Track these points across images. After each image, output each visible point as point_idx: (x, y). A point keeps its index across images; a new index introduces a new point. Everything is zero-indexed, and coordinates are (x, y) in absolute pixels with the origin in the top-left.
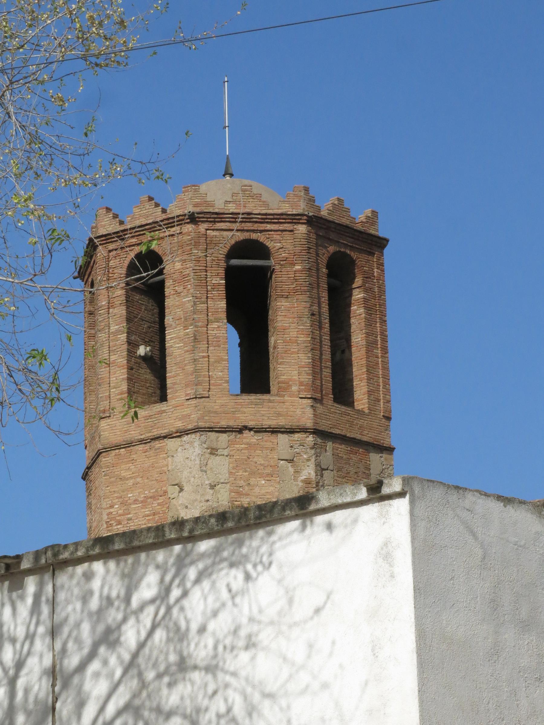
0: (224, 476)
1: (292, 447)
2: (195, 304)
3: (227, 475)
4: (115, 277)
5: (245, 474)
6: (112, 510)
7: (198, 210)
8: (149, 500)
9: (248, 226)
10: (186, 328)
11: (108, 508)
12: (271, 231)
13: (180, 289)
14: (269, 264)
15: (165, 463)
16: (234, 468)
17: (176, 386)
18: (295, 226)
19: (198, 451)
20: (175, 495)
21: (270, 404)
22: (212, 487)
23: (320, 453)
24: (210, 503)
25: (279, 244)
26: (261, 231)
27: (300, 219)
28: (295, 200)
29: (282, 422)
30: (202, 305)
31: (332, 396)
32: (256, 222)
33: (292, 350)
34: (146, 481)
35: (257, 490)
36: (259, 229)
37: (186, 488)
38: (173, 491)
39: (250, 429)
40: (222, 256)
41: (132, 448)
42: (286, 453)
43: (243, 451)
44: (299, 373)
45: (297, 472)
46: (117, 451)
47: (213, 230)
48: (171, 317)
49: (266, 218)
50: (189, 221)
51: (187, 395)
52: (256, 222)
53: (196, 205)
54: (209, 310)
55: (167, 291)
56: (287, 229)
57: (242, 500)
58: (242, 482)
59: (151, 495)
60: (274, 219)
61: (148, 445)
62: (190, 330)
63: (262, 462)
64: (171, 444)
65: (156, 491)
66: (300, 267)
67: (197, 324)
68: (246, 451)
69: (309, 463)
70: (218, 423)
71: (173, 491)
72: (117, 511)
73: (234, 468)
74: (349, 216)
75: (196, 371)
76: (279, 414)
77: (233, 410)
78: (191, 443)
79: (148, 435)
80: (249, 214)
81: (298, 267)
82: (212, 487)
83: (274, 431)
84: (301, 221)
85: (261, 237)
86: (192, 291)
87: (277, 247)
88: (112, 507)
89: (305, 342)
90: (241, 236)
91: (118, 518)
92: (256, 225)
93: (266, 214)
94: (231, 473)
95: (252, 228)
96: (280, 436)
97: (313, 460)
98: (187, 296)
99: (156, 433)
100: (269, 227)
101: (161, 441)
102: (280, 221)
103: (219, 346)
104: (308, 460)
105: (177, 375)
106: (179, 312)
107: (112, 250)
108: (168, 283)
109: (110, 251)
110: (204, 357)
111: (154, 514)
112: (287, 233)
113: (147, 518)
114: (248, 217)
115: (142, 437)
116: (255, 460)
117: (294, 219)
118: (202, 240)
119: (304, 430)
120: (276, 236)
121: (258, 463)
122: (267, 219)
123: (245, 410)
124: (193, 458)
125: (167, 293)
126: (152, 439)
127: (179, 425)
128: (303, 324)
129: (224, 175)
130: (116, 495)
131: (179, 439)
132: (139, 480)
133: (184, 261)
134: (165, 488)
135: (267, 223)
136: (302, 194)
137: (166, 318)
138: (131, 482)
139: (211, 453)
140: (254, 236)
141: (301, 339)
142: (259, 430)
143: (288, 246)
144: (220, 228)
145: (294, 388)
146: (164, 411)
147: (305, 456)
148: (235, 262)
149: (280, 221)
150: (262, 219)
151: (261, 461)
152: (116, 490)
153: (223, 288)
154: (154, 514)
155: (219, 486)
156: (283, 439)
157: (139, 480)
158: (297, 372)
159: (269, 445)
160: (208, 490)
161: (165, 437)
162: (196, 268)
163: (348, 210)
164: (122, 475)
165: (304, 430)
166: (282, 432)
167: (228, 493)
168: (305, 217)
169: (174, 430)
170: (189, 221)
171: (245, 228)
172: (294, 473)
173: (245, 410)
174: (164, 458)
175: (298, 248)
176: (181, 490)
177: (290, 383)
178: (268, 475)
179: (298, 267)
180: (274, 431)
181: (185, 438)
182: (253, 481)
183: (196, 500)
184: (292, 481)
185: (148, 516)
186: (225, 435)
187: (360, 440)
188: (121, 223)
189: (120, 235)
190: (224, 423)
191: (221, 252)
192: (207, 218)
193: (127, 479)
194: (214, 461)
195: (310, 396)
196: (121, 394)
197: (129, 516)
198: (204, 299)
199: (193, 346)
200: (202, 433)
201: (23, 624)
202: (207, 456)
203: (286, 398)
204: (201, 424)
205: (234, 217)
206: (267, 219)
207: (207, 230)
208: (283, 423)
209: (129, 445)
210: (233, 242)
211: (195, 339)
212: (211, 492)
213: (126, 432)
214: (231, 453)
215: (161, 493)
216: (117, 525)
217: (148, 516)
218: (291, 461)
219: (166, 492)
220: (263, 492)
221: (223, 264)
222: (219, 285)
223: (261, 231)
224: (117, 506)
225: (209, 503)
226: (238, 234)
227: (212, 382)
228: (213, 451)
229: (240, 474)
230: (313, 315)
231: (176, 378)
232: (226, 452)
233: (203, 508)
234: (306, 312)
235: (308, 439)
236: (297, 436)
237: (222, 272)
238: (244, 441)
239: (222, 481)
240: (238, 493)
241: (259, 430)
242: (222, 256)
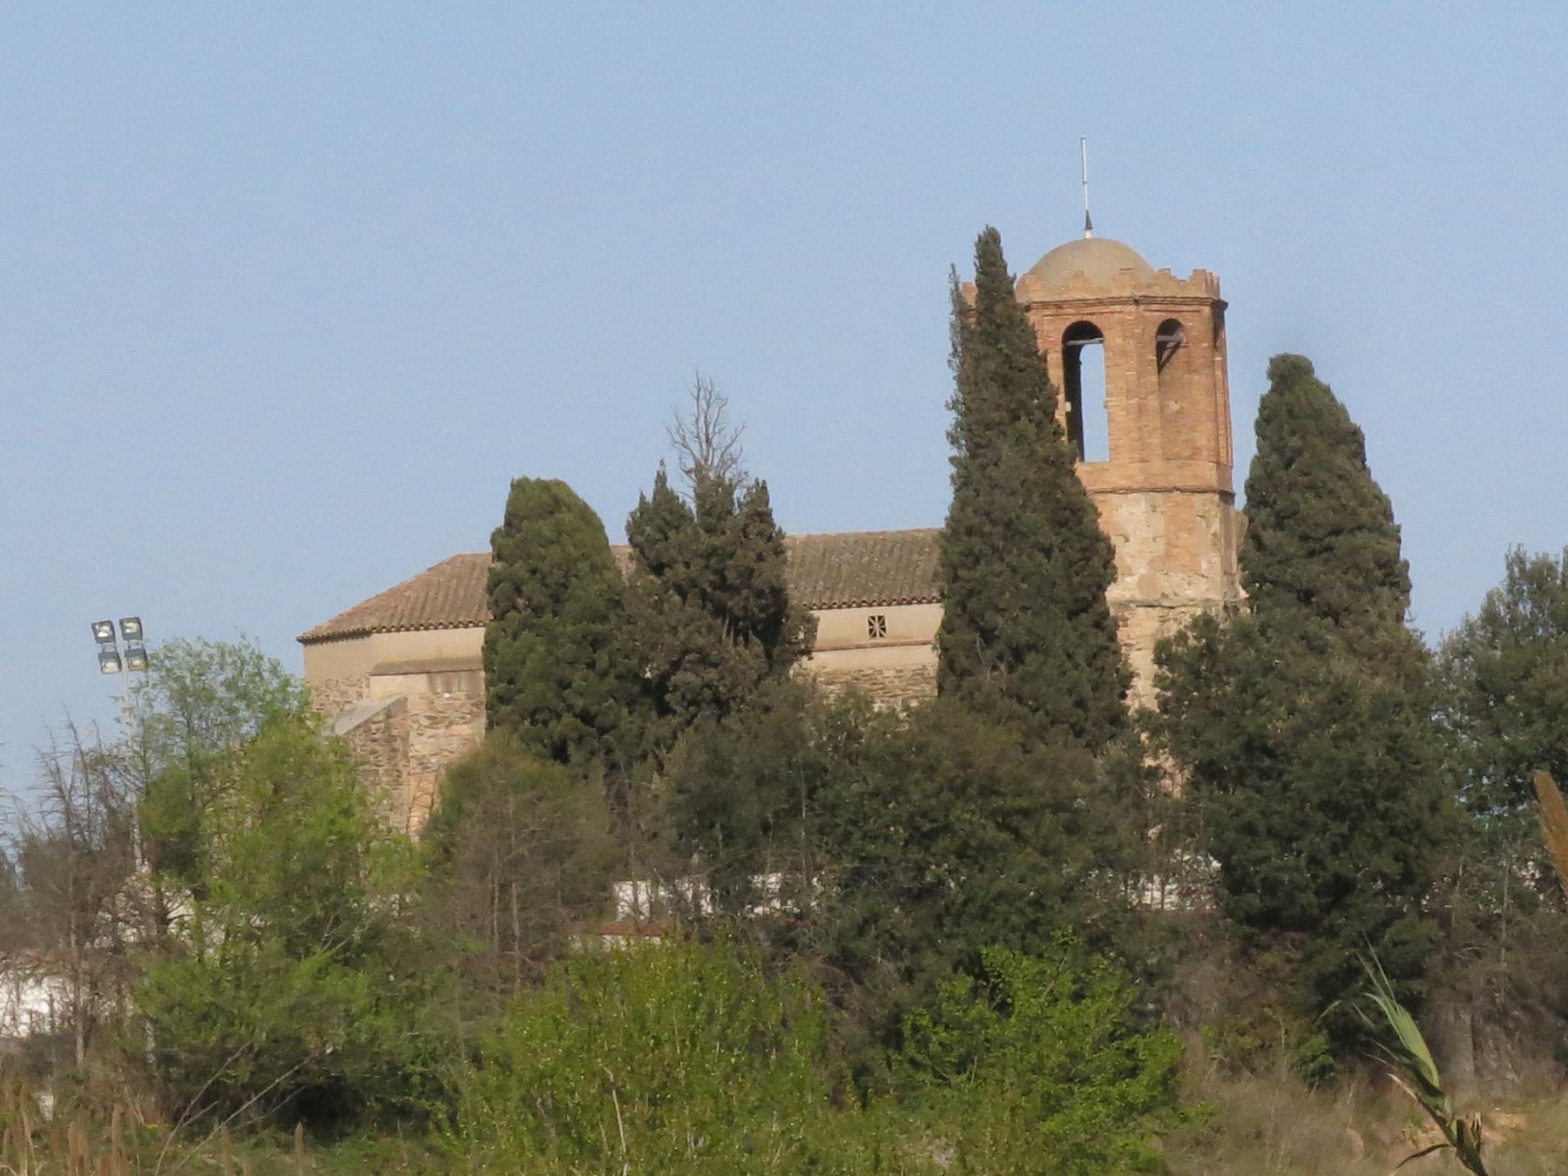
9: (1172, 308)
37: (1131, 539)
39: (1178, 490)
49: (1185, 301)
78: (1137, 501)
85: (1094, 320)
90: (1075, 319)
100: (1186, 308)
120: (1189, 315)
140: (1085, 318)
145: (1205, 453)
156: (1198, 498)
176: (1127, 540)
180: (1194, 492)
181: (1130, 496)
201: (1132, 596)
223: (1091, 314)
226: (1164, 314)
241: (1182, 491)
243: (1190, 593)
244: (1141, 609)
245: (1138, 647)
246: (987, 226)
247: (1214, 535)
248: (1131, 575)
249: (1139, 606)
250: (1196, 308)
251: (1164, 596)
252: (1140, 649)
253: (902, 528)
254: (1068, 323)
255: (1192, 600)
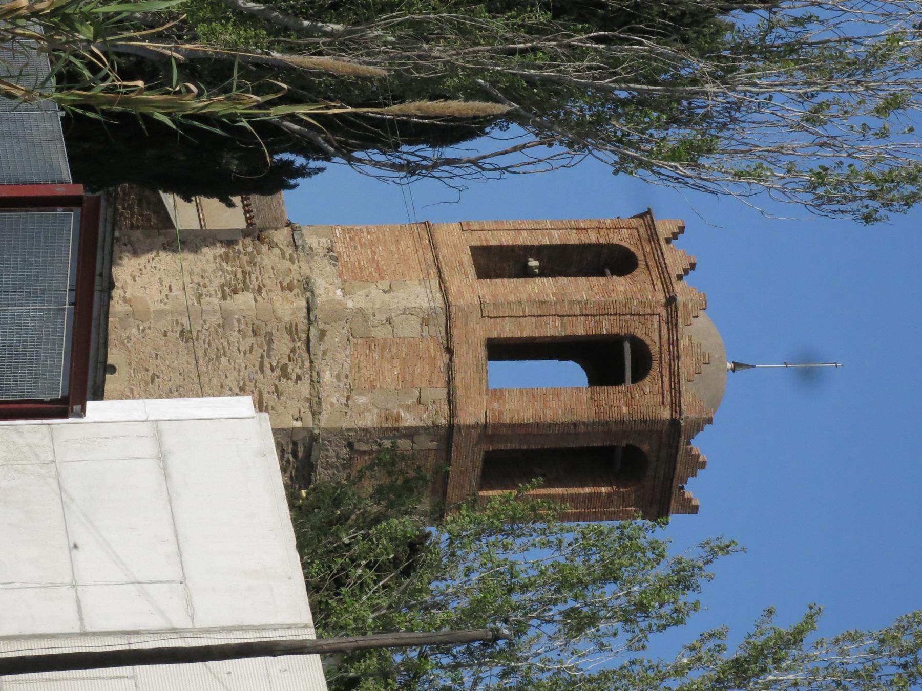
0: (400, 333)
1: (434, 402)
2: (579, 302)
3: (402, 336)
4: (610, 234)
5: (404, 354)
6: (365, 233)
7: (680, 308)
8: (375, 265)
9: (666, 357)
10: (554, 294)
11: (367, 229)
12: (662, 382)
13: (595, 289)
14: (627, 382)
15: (414, 278)
16: (409, 343)
17: (493, 287)
18: (668, 407)
19: (425, 305)
20: (380, 286)
21: (478, 380)
22: (389, 321)
23: (429, 434)
24: (372, 317)
25: (648, 390)
26: (661, 372)
27: (676, 412)
28: (696, 408)
29: (460, 392)
30: (578, 310)
31: (491, 449)
32: (670, 366)
33: (536, 403)
34: (395, 262)
35: (387, 366)
36: (664, 370)
37: (387, 295)
38: (385, 285)
39: (450, 360)
40: (632, 331)
41: (430, 249)
42: (427, 396)
43: (427, 352)
44: (511, 410)
45: (408, 408)
46: (426, 237)
47: (659, 321)
48: (566, 282)
49: (675, 375)
50: (668, 296)
51: (484, 296)
52: (670, 366)
53: (685, 305)
54: (574, 318)
55: (594, 280)
56: (665, 399)
57: (377, 349)
58: (395, 351)
59: (380, 266)
60: (675, 384)
61: (433, 263)
62: (552, 298)
63: (416, 372)
64: (435, 283)
65: (384, 271)
66: (624, 411)
67: (558, 305)
68: (427, 355)
69: (417, 419)
70: (455, 326)
71: (385, 285)
72: (364, 237)
73: (409, 343)
74: (688, 476)
75: (509, 303)
76: (467, 389)
77: (470, 342)
79: (443, 263)
80: (678, 358)
81: (624, 409)
82: (389, 321)
83: (450, 382)
84: (674, 413)
86: (593, 299)
87: (645, 389)
88: (368, 233)
89: (545, 416)
91: (357, 238)
92: (667, 367)
93: (678, 375)
94: (404, 338)
95: (663, 362)
96: (445, 390)
97: (421, 424)
98: (587, 295)
99: (445, 270)
100: (666, 380)
101: (436, 275)
102: (673, 390)
103: (536, 327)
104: (421, 419)
105: (505, 287)
106: (571, 289)
107: (638, 232)
108: (602, 280)
109: (637, 229)
110: (524, 311)
111: (361, 269)
112: (661, 400)
113: (357, 263)
114: (675, 357)
115: (441, 258)
116: (418, 364)
117: (676, 405)
118: (648, 311)
119: (452, 414)
120: (657, 388)
121: (416, 368)
122: (674, 376)
123: (471, 354)
124: (418, 301)
125: (591, 279)
126: (438, 266)
127: (453, 290)
128: (563, 414)
129: (733, 362)
130: (381, 236)
131: (438, 290)
132: (396, 256)
133: (625, 293)
134: (387, 278)
135: (670, 378)
136: (704, 416)
137: (565, 278)
138: (394, 249)
139: (423, 319)
140: (655, 364)
141: (548, 412)
142: (450, 366)
143: (646, 399)
144: (662, 328)
145: (496, 405)
146: (467, 277)
147: (425, 416)
148: (627, 347)
149: (673, 390)
150: (674, 372)
151: (418, 370)
152: (386, 237)
153: (598, 331)
154: (361, 269)
155: (390, 328)
156: (442, 393)
157: (396, 256)
158: (513, 407)
159: (435, 379)
160: (385, 316)
161: (440, 277)
162: (617, 303)
163: (694, 474)
164: (402, 242)
165: (452, 414)
166: (449, 393)
167: (383, 337)
168: (678, 416)
169: (447, 285)
170: (668, 296)
171: (663, 355)
172: (407, 405)
173: (471, 354)
174: (418, 277)
175: (644, 410)
176: (385, 292)
177: (501, 401)
178: (404, 377)
179: (624, 409)
180: (450, 382)
182: (396, 362)
183: (374, 304)
184: (398, 403)
185: (359, 264)
186: (443, 333)
187: (447, 483)
188: (668, 241)
189: (653, 237)
190: (455, 332)
191: (636, 330)
192: (671, 315)
193: (397, 246)
194: (415, 322)
195: (488, 421)
196: (486, 240)
197: (359, 248)
198: (585, 312)
199: (534, 301)
200: (444, 309)
202: (421, 315)
203: (485, 397)
204: (453, 309)
205: (674, 343)
206: (674, 376)
207: (659, 315)
208: (458, 394)
209: (433, 246)
210: (648, 342)
211: (543, 302)
212: (384, 319)
213: (447, 245)
214: (424, 340)
215: (382, 275)
216: (350, 237)
217: (359, 264)
218: (419, 402)
219: (383, 278)
220: (386, 373)
221: (623, 332)
222: (602, 328)
223: (661, 372)
224: (369, 237)
225: (372, 317)
226: (657, 348)
227: (498, 320)
228: (425, 321)
229: (404, 349)
230: (575, 425)
231: (502, 286)
232: (425, 334)
233: (366, 311)
234: (576, 418)
235: (443, 419)
236: (446, 408)
237: (615, 331)
238: (439, 354)
239: (395, 330)
240: (384, 346)
241: (450, 366)
242: (632, 331)
243: (327, 377)
244: (304, 304)
245: (259, 298)
246: (685, 624)
247: (398, 418)
248: (345, 294)
249: (308, 299)
250: (668, 399)
251: (323, 333)
252: (256, 301)
253: (285, 496)
254: (633, 249)
255: (318, 374)
